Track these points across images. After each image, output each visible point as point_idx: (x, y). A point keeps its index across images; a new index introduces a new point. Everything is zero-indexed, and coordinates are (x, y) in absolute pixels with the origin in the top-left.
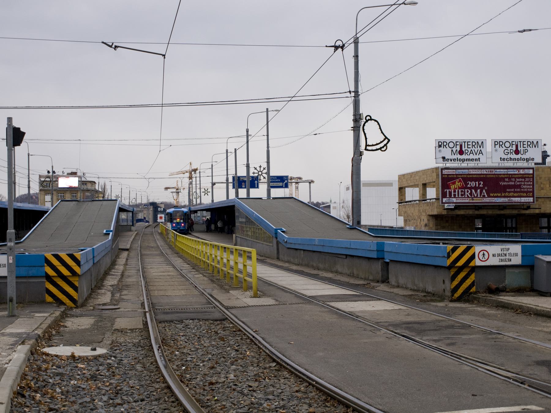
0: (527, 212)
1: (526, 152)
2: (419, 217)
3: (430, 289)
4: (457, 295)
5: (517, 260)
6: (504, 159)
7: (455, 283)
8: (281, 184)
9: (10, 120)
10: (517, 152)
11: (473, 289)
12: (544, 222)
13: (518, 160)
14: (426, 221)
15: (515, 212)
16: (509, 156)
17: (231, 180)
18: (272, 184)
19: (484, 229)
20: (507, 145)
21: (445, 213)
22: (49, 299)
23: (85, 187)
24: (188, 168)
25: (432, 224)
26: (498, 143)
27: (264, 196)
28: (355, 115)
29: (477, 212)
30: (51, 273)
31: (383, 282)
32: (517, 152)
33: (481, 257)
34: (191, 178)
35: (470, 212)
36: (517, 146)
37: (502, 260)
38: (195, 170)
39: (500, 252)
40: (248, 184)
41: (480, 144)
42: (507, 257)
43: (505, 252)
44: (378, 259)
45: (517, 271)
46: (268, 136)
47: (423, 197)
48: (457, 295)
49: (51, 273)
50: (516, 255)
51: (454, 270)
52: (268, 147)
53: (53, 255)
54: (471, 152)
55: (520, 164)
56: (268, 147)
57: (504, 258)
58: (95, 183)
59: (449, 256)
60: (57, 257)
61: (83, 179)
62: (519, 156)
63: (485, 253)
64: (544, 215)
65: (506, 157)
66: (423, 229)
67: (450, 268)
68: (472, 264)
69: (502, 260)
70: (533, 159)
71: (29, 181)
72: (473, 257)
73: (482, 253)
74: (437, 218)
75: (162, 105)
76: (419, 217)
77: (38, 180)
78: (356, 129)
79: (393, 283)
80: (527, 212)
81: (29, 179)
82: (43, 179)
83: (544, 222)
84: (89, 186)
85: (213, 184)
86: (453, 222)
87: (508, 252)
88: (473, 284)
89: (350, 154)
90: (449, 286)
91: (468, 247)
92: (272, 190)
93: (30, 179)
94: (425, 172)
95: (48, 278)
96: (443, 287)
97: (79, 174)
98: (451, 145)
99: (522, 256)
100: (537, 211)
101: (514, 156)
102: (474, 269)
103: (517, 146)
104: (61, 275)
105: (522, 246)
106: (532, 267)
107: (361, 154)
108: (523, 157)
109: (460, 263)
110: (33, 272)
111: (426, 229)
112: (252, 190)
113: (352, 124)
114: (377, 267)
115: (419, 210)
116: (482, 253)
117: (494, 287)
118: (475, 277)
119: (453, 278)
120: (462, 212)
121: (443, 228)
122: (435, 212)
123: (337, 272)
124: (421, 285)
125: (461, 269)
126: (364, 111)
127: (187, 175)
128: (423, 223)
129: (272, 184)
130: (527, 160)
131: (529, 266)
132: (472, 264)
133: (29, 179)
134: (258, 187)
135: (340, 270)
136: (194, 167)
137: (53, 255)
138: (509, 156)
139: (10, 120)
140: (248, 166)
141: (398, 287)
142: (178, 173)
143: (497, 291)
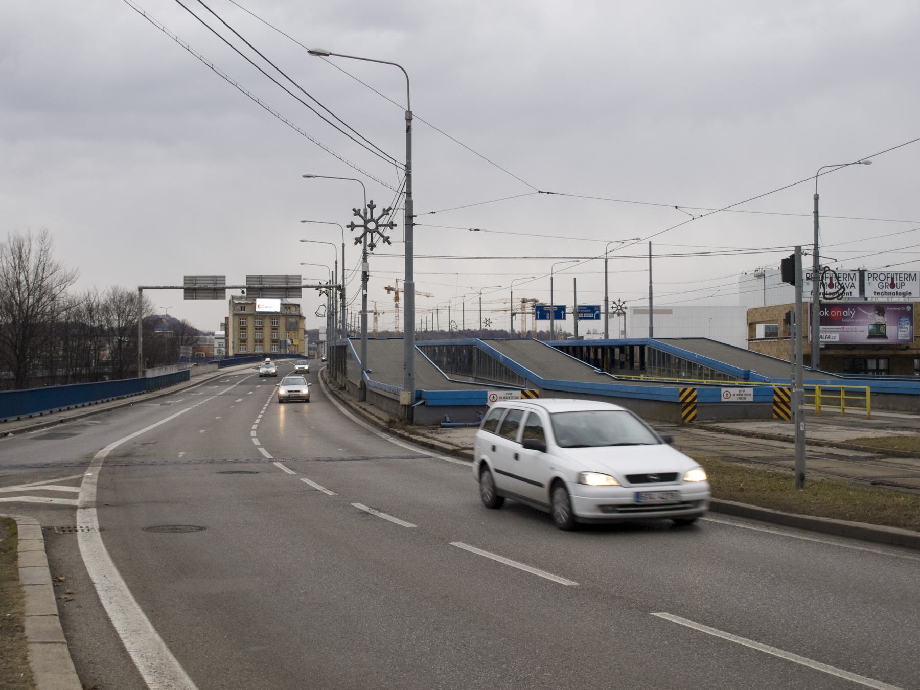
0: (904, 353)
1: (902, 285)
6: (878, 294)
8: (591, 315)
10: (893, 285)
13: (894, 294)
15: (891, 352)
16: (884, 290)
17: (602, 316)
18: (581, 315)
19: (888, 371)
20: (882, 277)
22: (775, 416)
23: (288, 312)
27: (571, 331)
32: (893, 285)
36: (893, 279)
40: (552, 315)
46: (650, 270)
52: (651, 282)
55: (895, 299)
56: (651, 282)
60: (781, 390)
62: (895, 290)
65: (880, 291)
70: (910, 294)
75: (650, 256)
80: (904, 353)
82: (236, 301)
84: (293, 311)
92: (580, 323)
95: (775, 402)
100: (915, 352)
101: (890, 290)
103: (893, 279)
104: (783, 402)
108: (900, 291)
109: (688, 400)
110: (767, 399)
112: (557, 323)
115: (779, 350)
120: (831, 352)
129: (581, 315)
130: (904, 295)
134: (564, 319)
138: (884, 290)
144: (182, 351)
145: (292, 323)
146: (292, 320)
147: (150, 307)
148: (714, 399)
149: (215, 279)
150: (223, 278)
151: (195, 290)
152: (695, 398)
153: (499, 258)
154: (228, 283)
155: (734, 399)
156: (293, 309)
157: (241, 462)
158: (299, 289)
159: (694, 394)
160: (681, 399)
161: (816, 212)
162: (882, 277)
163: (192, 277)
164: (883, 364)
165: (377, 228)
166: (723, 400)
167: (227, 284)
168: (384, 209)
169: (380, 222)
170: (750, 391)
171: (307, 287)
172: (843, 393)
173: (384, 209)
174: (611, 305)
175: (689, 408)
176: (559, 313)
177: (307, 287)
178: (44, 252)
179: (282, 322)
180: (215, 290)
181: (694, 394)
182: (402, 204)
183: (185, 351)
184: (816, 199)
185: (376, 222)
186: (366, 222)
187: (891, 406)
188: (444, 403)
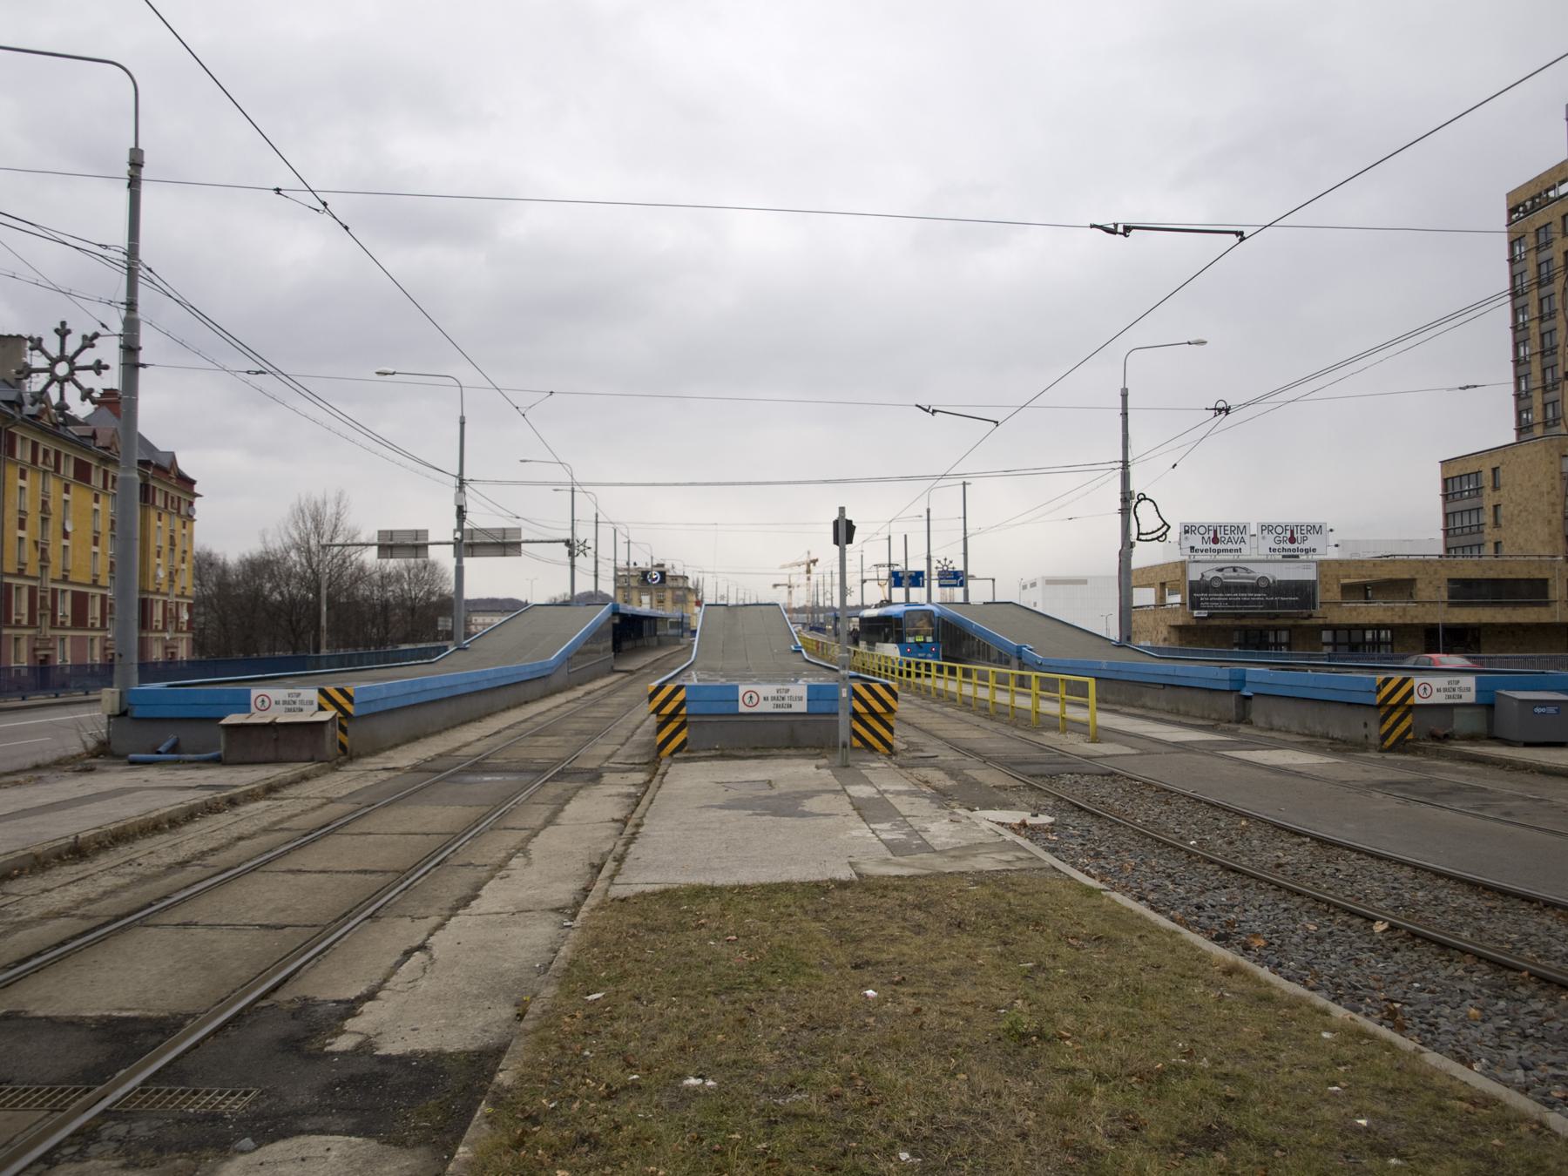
0: (1307, 622)
1: (1304, 539)
2: (1155, 628)
3: (1337, 733)
4: (1388, 743)
5: (1470, 697)
7: (1386, 727)
9: (842, 510)
10: (1292, 540)
11: (1410, 736)
12: (1326, 636)
14: (1165, 633)
19: (1289, 646)
20: (1279, 530)
21: (1193, 622)
22: (857, 743)
24: (805, 559)
25: (1174, 637)
26: (1266, 528)
28: (1123, 493)
29: (1237, 622)
30: (861, 708)
31: (1238, 722)
32: (1292, 540)
34: (808, 571)
35: (1229, 622)
38: (814, 562)
41: (1241, 529)
44: (1231, 691)
45: (1468, 711)
47: (1161, 602)
48: (1388, 743)
49: (861, 708)
50: (1469, 690)
51: (1384, 709)
54: (1230, 540)
59: (1379, 691)
62: (1295, 546)
64: (1327, 627)
66: (1161, 644)
67: (1379, 707)
68: (1409, 702)
72: (1411, 692)
74: (1181, 630)
76: (1155, 628)
77: (612, 574)
78: (1126, 510)
79: (1261, 724)
80: (1307, 622)
83: (1326, 636)
84: (680, 583)
85: (864, 581)
86: (1192, 635)
88: (1408, 730)
89: (1117, 545)
90: (1375, 731)
94: (1163, 567)
96: (1365, 731)
98: (1202, 530)
100: (1321, 621)
101: (1288, 546)
102: (1412, 708)
105: (1478, 682)
106: (1490, 707)
107: (1132, 545)
109: (1394, 701)
111: (1166, 645)
112: (913, 590)
113: (1119, 505)
114: (1232, 701)
117: (1441, 732)
119: (1383, 721)
120: (1217, 622)
121: (1190, 643)
122: (1180, 622)
123: (1143, 707)
124: (1319, 729)
125: (1394, 707)
126: (1136, 486)
127: (804, 568)
128: (1161, 637)
131: (1487, 705)
132: (1409, 702)
135: (1149, 704)
136: (813, 557)
139: (842, 510)
140: (929, 559)
141: (1272, 729)
142: (791, 566)
143: (1447, 737)
146: (680, 593)
148: (724, 708)
149: (417, 533)
151: (391, 547)
152: (682, 704)
154: (431, 539)
155: (767, 707)
158: (518, 544)
159: (680, 696)
161: (1125, 414)
162: (1279, 530)
164: (1284, 637)
165: (72, 372)
166: (742, 708)
167: (431, 539)
168: (84, 337)
169: (80, 361)
172: (1062, 688)
173: (84, 337)
174: (934, 564)
175: (672, 726)
176: (916, 579)
178: (338, 515)
180: (416, 547)
181: (680, 696)
182: (117, 327)
183: (444, 623)
184: (1125, 395)
185: (71, 361)
186: (62, 358)
187: (1182, 708)
188: (167, 714)
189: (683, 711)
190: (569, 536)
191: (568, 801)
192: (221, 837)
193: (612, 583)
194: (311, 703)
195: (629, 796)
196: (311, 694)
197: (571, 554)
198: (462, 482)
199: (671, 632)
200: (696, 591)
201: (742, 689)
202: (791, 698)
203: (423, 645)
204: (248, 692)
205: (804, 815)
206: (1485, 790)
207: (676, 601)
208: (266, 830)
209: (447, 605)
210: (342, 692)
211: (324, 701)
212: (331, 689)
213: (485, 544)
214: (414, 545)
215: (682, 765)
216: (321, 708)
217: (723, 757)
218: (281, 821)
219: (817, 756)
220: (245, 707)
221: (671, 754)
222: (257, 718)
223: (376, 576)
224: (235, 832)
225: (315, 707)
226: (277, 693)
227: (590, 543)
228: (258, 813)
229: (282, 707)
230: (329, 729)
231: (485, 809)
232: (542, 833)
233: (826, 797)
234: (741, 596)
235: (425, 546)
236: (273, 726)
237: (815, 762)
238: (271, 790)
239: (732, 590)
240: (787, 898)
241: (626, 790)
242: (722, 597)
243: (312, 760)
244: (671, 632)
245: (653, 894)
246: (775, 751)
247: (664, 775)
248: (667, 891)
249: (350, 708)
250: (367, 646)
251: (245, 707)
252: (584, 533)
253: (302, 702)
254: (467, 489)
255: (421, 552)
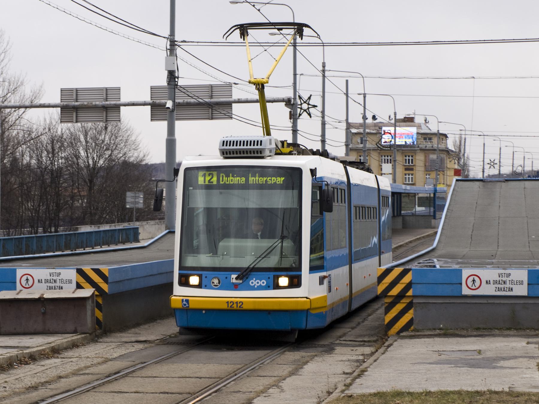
23: (429, 145)
33: (470, 284)
37: (499, 289)
39: (49, 278)
42: (58, 284)
43: (55, 278)
50: (521, 283)
53: (93, 269)
57: (53, 285)
58: (446, 136)
61: (424, 130)
63: (30, 278)
69: (499, 289)
71: (324, 124)
73: (471, 279)
81: (323, 117)
82: (354, 131)
87: (59, 278)
91: (405, 269)
93: (326, 118)
97: (417, 120)
99: (528, 284)
109: (395, 291)
116: (471, 279)
118: (414, 314)
133: (323, 117)
137: (93, 269)
144: (129, 199)
145: (433, 161)
146: (433, 157)
147: (133, 138)
148: (447, 291)
150: (118, 90)
151: (76, 109)
152: (409, 286)
153: (355, 44)
154: (124, 99)
156: (435, 140)
157: (66, 377)
158: (229, 105)
160: (381, 289)
163: (71, 90)
166: (465, 291)
167: (124, 99)
170: (522, 275)
171: (239, 101)
175: (399, 307)
177: (239, 101)
179: (420, 159)
180: (106, 108)
181: (407, 279)
183: (135, 200)
189: (410, 293)
190: (289, 93)
191: (306, 363)
192: (53, 373)
193: (344, 148)
194: (70, 282)
195: (357, 361)
196: (71, 274)
197: (294, 117)
198: (173, 44)
199: (419, 209)
200: (457, 154)
201: (466, 273)
202: (512, 282)
203: (106, 227)
204: (14, 272)
205: (494, 368)
206: (401, 246)
207: (429, 168)
208: (75, 373)
209: (134, 174)
210: (98, 272)
211: (82, 280)
212: (87, 269)
213: (188, 105)
214: (104, 107)
215: (407, 341)
216: (79, 286)
217: (445, 335)
218: (87, 367)
219: (528, 336)
220: (11, 285)
221: (398, 333)
222: (24, 295)
223: (45, 139)
224: (61, 371)
225: (74, 285)
226: (40, 273)
227: (316, 100)
228: (51, 367)
229: (44, 285)
230: (89, 305)
231: (239, 366)
232: (288, 379)
233: (521, 359)
234: (518, 162)
235: (117, 108)
236: (41, 301)
237: (527, 340)
238: (55, 351)
239: (507, 154)
240: (456, 397)
241: (355, 358)
242: (492, 164)
243: (75, 332)
244: (419, 209)
245: (370, 395)
246: (497, 332)
247: (389, 346)
248: (379, 393)
249: (105, 287)
250: (34, 227)
251: (11, 285)
252: (309, 87)
253: (62, 281)
254: (179, 51)
255: (112, 115)
